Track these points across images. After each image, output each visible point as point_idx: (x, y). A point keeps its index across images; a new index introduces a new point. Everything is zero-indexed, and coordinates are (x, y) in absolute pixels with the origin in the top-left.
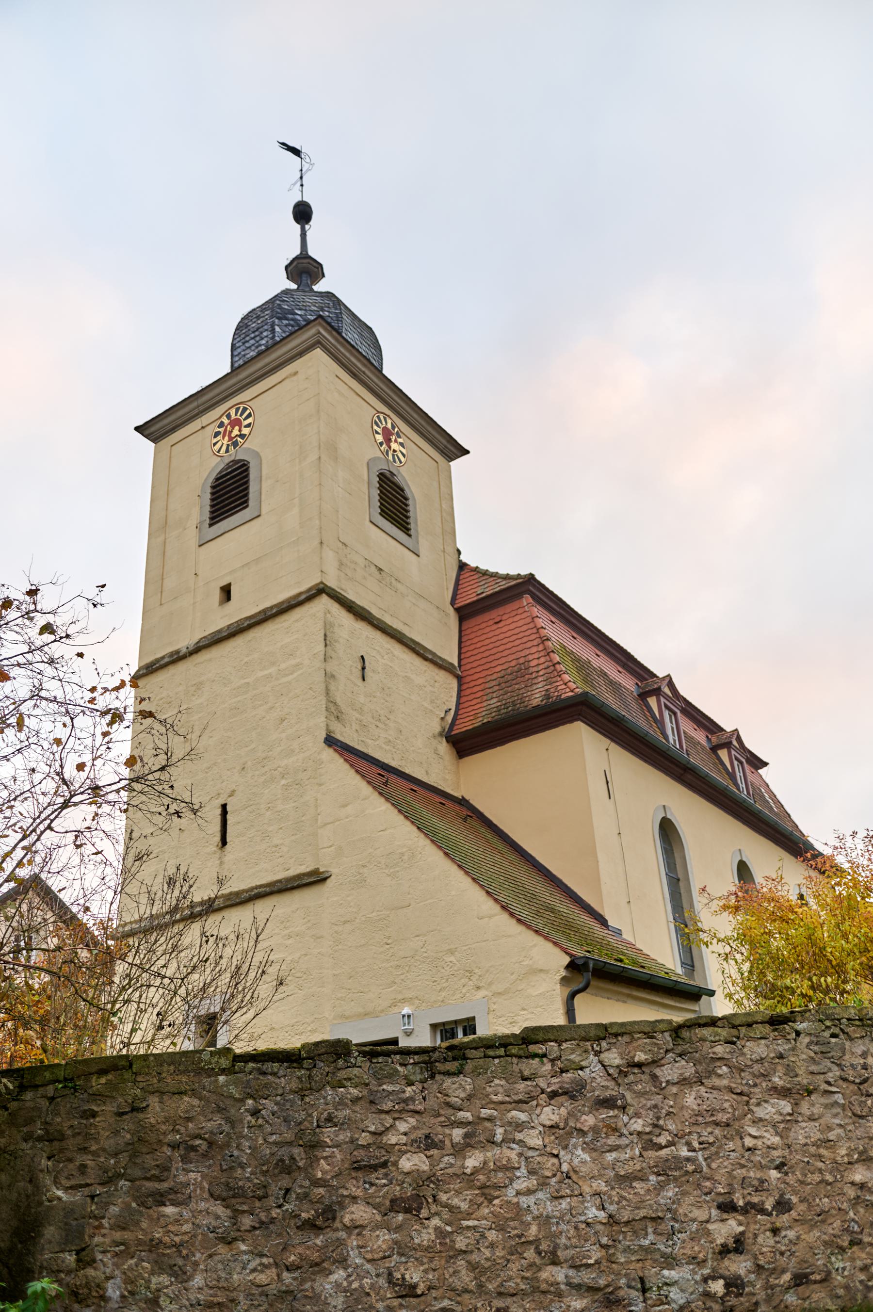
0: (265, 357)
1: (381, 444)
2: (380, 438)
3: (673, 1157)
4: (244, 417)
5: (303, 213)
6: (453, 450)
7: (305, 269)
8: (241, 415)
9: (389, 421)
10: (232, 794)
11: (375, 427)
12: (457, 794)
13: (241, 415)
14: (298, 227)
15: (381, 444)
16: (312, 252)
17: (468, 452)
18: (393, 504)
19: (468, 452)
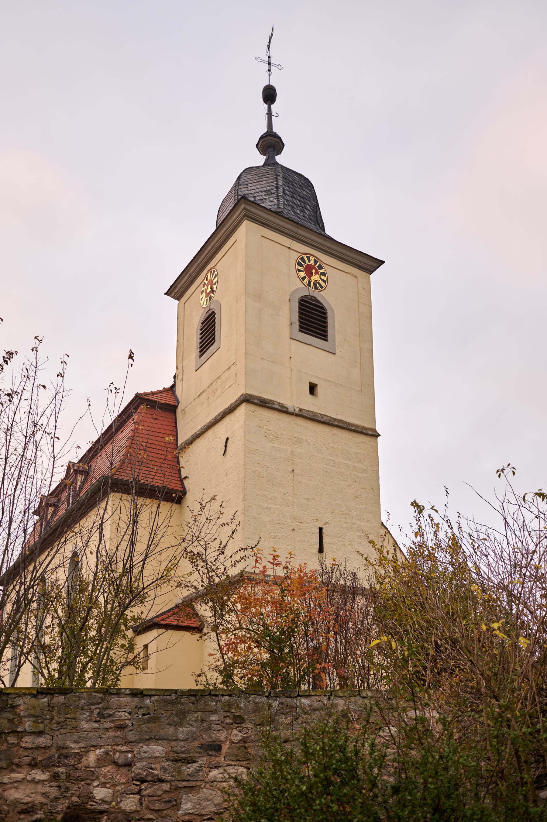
0: (278, 219)
1: (304, 278)
2: (302, 274)
3: (385, 633)
4: (307, 261)
5: (269, 95)
6: (369, 264)
7: (271, 144)
8: (305, 263)
9: (216, 279)
10: (326, 524)
11: (299, 267)
12: (20, 673)
13: (305, 263)
14: (266, 106)
15: (304, 278)
16: (274, 130)
17: (383, 262)
18: (313, 319)
19: (383, 262)
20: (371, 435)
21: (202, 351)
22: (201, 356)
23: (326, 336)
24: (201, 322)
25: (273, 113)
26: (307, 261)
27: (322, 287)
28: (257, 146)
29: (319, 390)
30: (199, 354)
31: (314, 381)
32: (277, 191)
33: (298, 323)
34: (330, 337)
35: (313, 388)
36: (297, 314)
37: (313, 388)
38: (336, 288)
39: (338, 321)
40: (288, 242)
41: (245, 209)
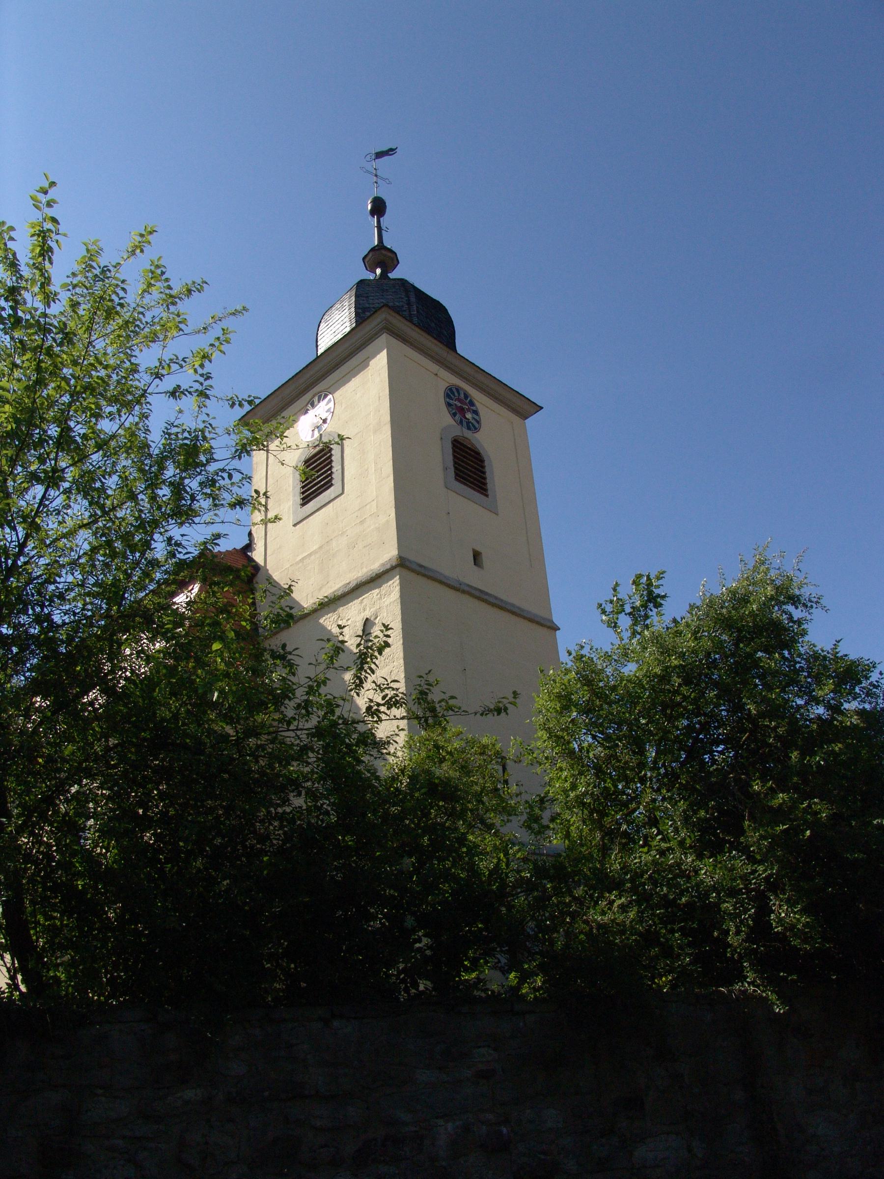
4: (456, 394)
5: (379, 208)
17: (542, 408)
19: (542, 408)
20: (550, 628)
21: (305, 500)
22: (303, 505)
23: (486, 490)
24: (303, 459)
25: (384, 228)
26: (456, 394)
27: (476, 429)
28: (364, 259)
29: (485, 560)
30: (299, 501)
31: (478, 549)
32: (409, 308)
33: (453, 469)
34: (489, 492)
35: (477, 557)
36: (451, 457)
37: (477, 557)
38: (492, 434)
39: (498, 473)
40: (435, 368)
41: (386, 319)
